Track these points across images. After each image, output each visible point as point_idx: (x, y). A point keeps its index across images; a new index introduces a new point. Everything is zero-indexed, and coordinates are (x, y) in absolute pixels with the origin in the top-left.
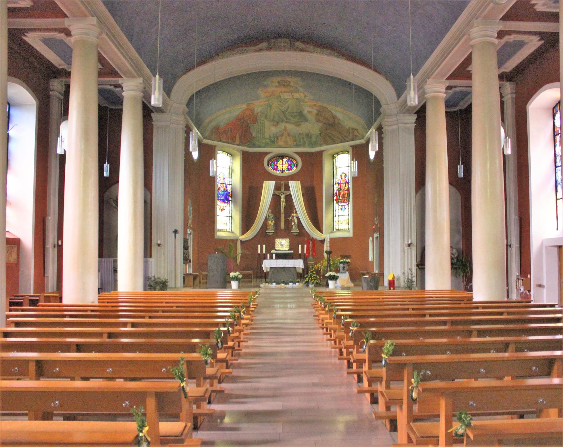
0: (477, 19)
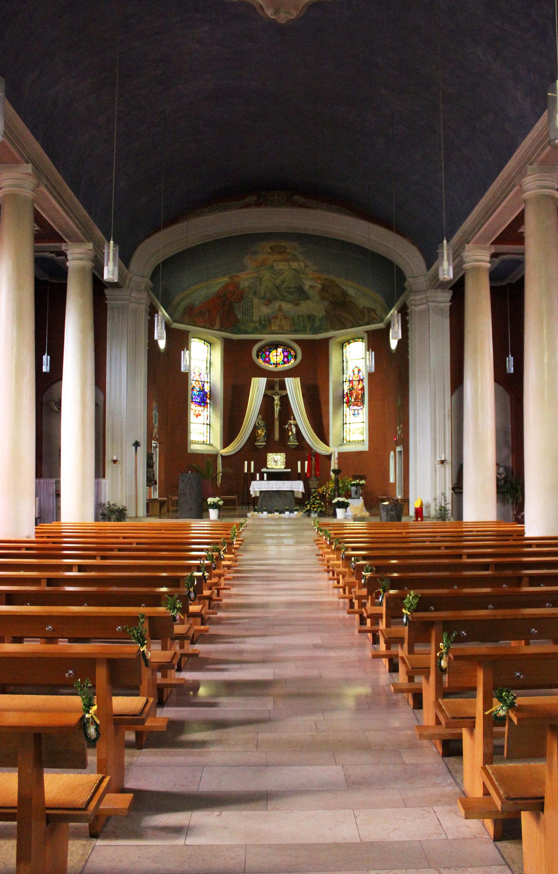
0: (531, 164)
